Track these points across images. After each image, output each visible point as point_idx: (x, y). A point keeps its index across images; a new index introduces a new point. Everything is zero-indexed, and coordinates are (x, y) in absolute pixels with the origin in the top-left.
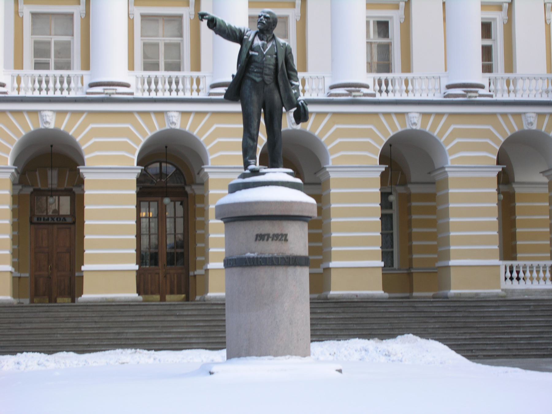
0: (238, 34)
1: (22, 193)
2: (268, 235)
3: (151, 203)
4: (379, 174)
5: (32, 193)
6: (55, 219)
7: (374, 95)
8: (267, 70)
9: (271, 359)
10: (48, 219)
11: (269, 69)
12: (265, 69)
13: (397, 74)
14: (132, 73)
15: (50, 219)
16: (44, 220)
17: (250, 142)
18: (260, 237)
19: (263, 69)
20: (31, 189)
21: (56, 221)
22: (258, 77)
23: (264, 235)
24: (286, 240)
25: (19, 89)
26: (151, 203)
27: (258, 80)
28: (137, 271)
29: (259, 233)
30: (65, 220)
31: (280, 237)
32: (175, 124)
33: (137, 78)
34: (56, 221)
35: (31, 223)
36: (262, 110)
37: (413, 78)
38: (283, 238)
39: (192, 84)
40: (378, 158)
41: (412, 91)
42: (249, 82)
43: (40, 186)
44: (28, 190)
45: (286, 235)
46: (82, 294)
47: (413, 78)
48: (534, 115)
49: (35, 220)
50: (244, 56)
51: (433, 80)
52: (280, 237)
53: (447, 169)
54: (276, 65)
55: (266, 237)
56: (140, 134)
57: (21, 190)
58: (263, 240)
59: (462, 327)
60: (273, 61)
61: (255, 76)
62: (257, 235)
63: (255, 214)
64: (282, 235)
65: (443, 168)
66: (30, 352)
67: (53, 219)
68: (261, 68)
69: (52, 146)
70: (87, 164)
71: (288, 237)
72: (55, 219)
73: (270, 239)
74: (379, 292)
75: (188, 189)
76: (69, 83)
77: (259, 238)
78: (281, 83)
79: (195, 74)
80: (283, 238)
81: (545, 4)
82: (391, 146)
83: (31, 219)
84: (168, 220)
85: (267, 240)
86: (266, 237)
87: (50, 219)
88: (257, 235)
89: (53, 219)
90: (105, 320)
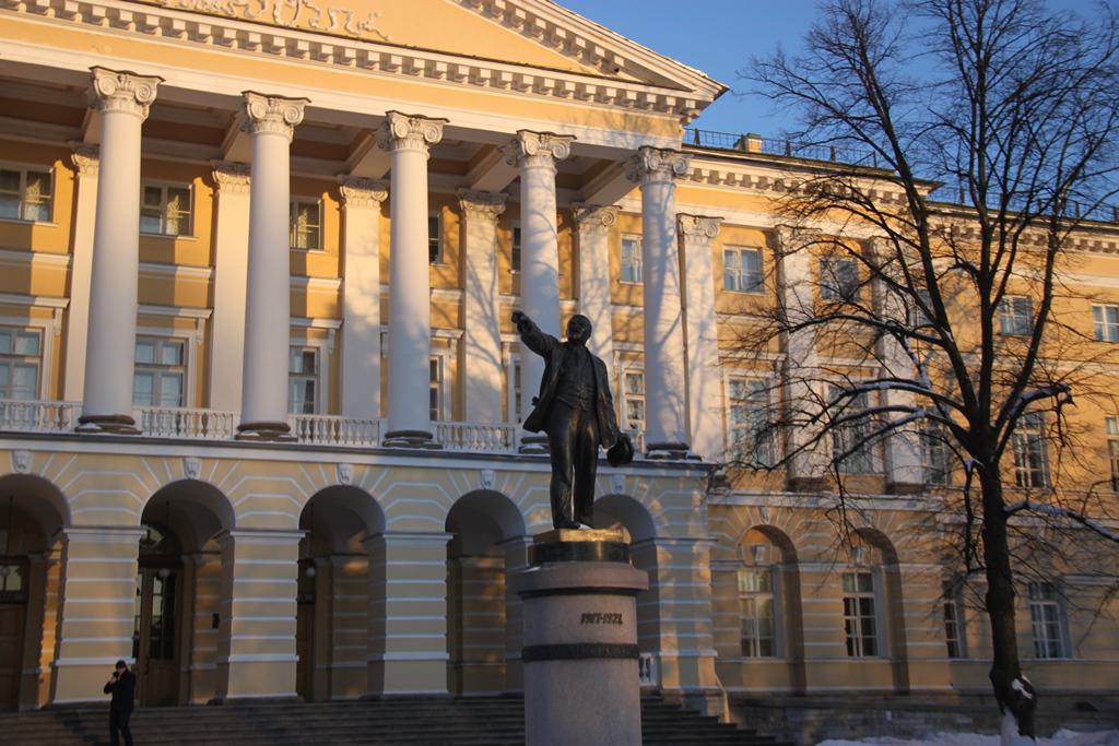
2: (598, 615)
4: (298, 541)
7: (296, 440)
9: (890, 743)
13: (322, 416)
14: (433, 422)
24: (620, 622)
25: (205, 431)
28: (448, 662)
29: (586, 612)
32: (25, 467)
33: (298, 420)
37: (160, 411)
39: (196, 423)
40: (444, 523)
41: (185, 430)
45: (620, 615)
47: (160, 411)
48: (623, 477)
51: (362, 425)
53: (384, 536)
56: (145, 486)
58: (592, 622)
62: (584, 615)
63: (563, 586)
64: (616, 615)
65: (380, 534)
66: (840, 738)
71: (622, 619)
73: (601, 621)
74: (446, 691)
75: (185, 559)
76: (337, 430)
79: (202, 411)
81: (381, 334)
82: (312, 505)
84: (155, 598)
85: (598, 622)
88: (584, 615)
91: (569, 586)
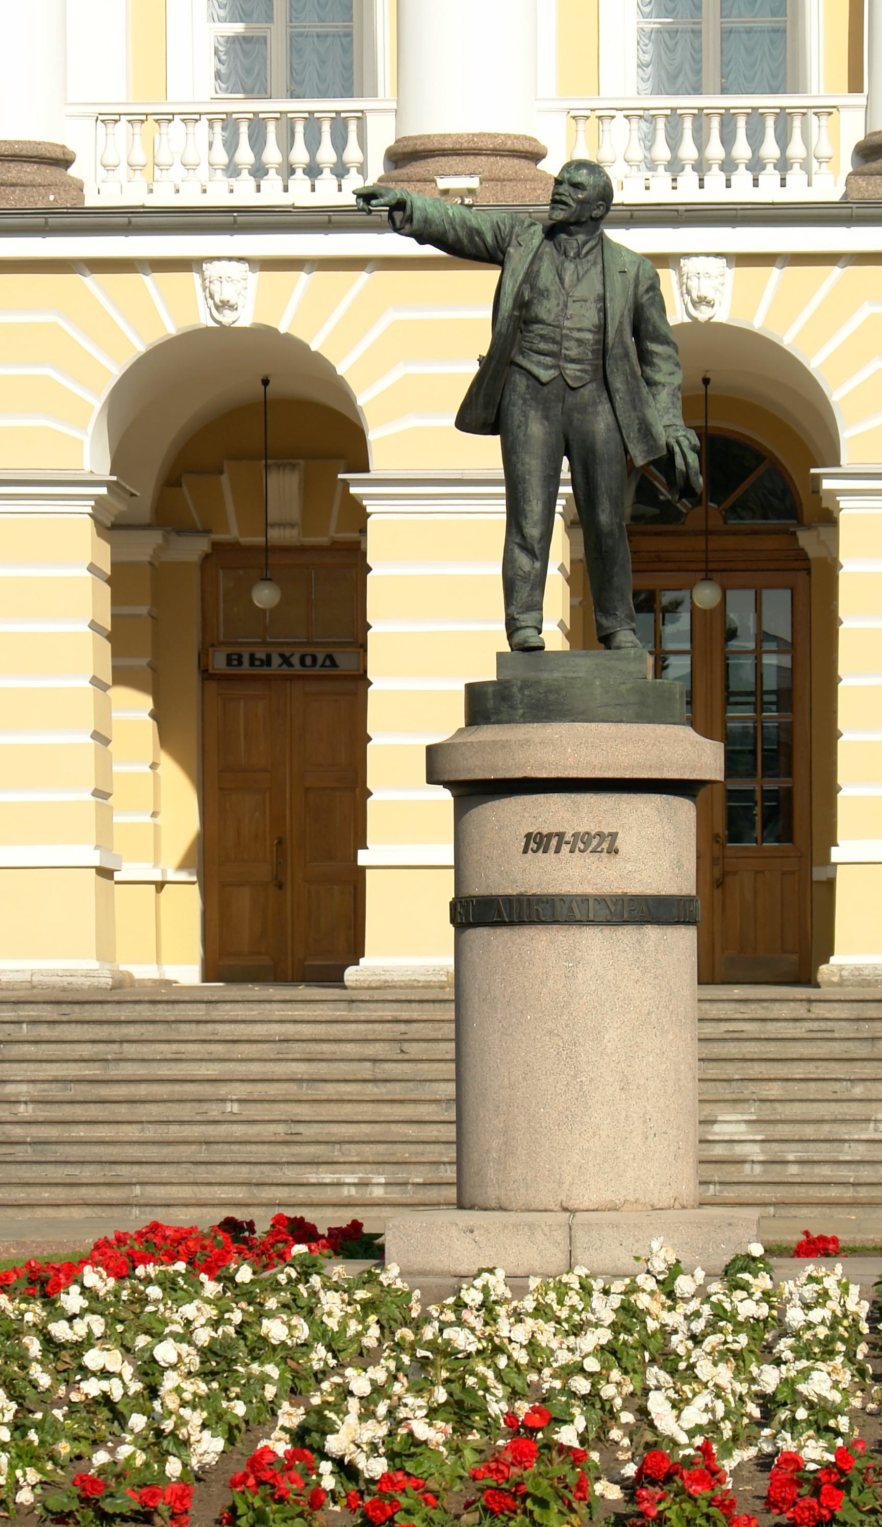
0: (489, 238)
1: (170, 556)
3: (767, 594)
5: (206, 557)
6: (295, 660)
8: (573, 344)
10: (268, 662)
11: (580, 342)
12: (566, 344)
15: (276, 660)
16: (252, 664)
17: (523, 561)
18: (538, 842)
19: (559, 343)
20: (202, 545)
21: (298, 669)
22: (547, 367)
23: (550, 836)
24: (613, 851)
26: (767, 594)
27: (545, 375)
29: (534, 829)
30: (334, 664)
31: (595, 842)
34: (298, 669)
35: (206, 675)
36: (565, 462)
38: (605, 846)
42: (521, 383)
43: (233, 533)
44: (193, 549)
45: (614, 836)
46: (832, 954)
49: (219, 662)
50: (507, 304)
52: (595, 842)
54: (602, 328)
55: (554, 842)
57: (159, 550)
59: (271, 1060)
60: (591, 317)
61: (539, 364)
62: (528, 836)
67: (286, 661)
68: (554, 342)
69: (266, 382)
70: (381, 461)
72: (295, 660)
73: (565, 848)
77: (533, 845)
78: (618, 383)
80: (607, 844)
83: (203, 657)
85: (557, 851)
86: (554, 842)
87: (276, 660)
88: (528, 836)
89: (286, 661)
90: (414, 1050)
91: (508, 775)
